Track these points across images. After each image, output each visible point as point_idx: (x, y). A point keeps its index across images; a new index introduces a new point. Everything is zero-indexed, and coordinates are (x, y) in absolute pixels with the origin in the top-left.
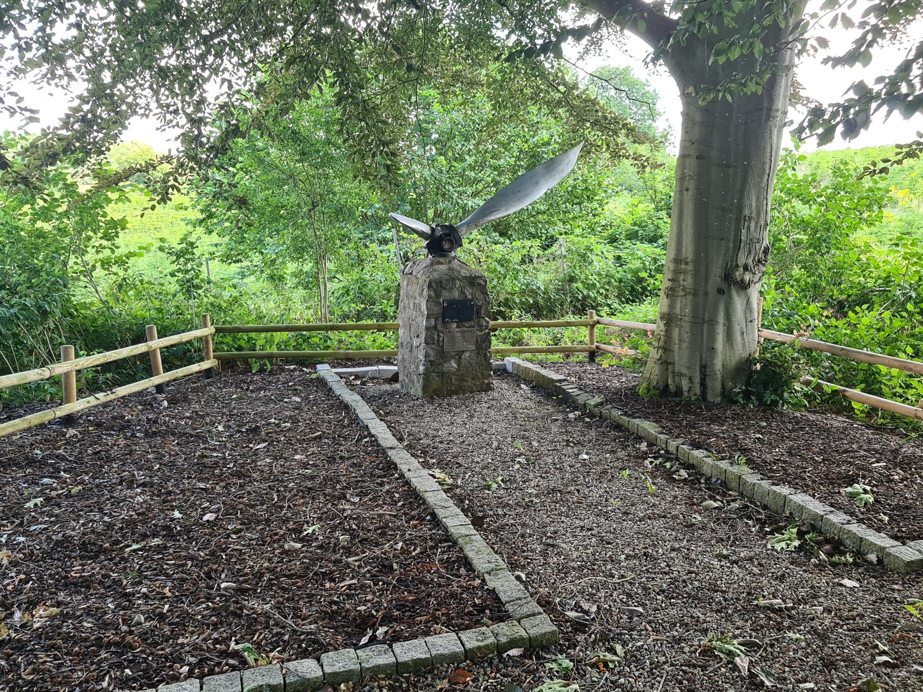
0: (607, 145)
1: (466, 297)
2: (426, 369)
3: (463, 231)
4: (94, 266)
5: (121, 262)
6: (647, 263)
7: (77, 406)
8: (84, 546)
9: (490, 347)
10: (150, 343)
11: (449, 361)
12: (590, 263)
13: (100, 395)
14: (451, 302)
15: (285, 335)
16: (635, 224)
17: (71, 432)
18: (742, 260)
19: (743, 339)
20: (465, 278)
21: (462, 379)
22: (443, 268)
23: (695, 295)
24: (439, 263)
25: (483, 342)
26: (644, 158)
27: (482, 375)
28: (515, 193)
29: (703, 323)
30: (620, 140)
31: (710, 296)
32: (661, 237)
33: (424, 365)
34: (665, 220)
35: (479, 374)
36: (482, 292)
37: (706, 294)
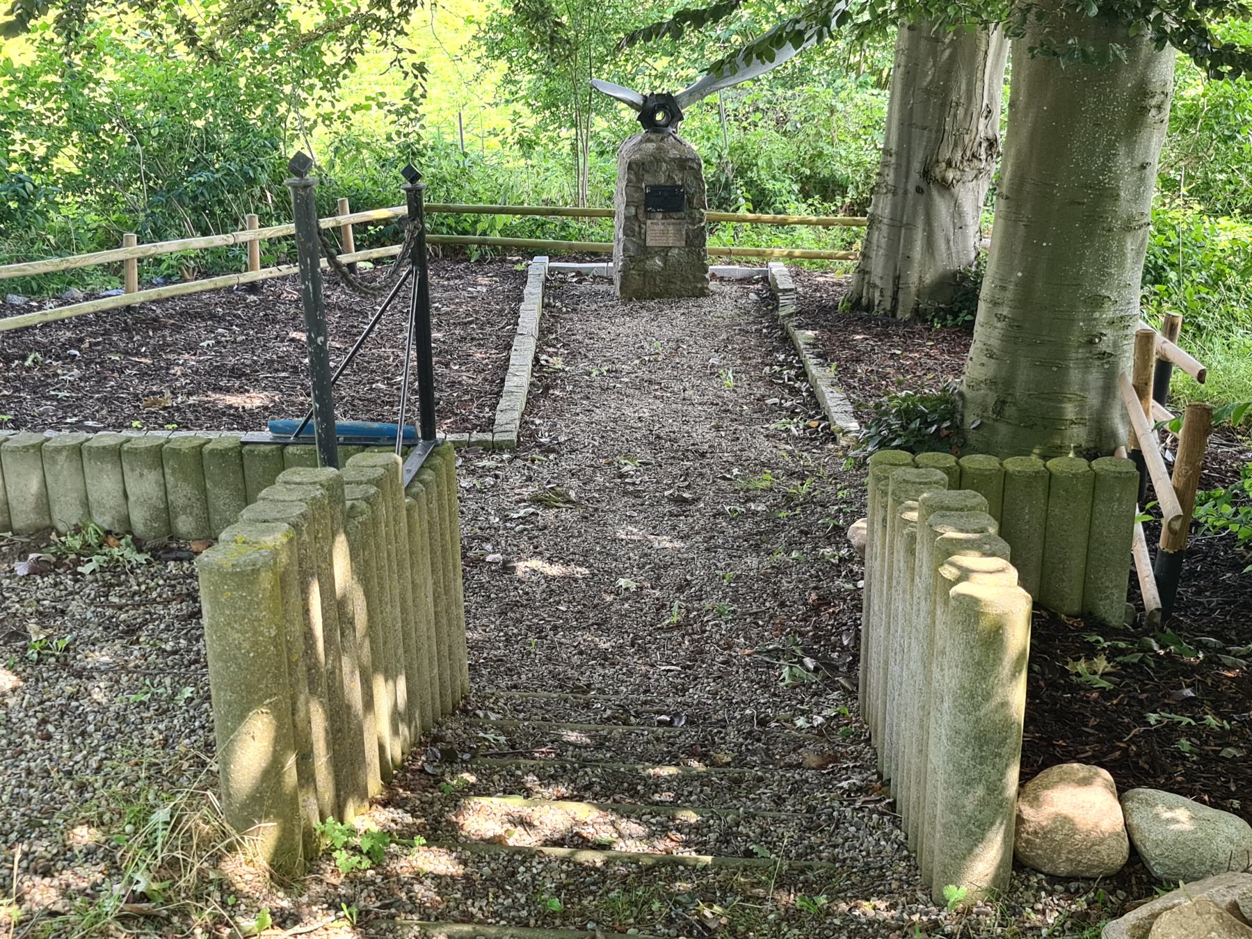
4: (315, 122)
5: (343, 117)
7: (258, 274)
8: (232, 370)
10: (339, 218)
11: (653, 258)
13: (283, 267)
14: (655, 189)
15: (516, 220)
17: (252, 298)
18: (946, 154)
19: (949, 248)
20: (674, 160)
22: (651, 146)
23: (895, 194)
29: (901, 227)
31: (910, 196)
37: (906, 192)
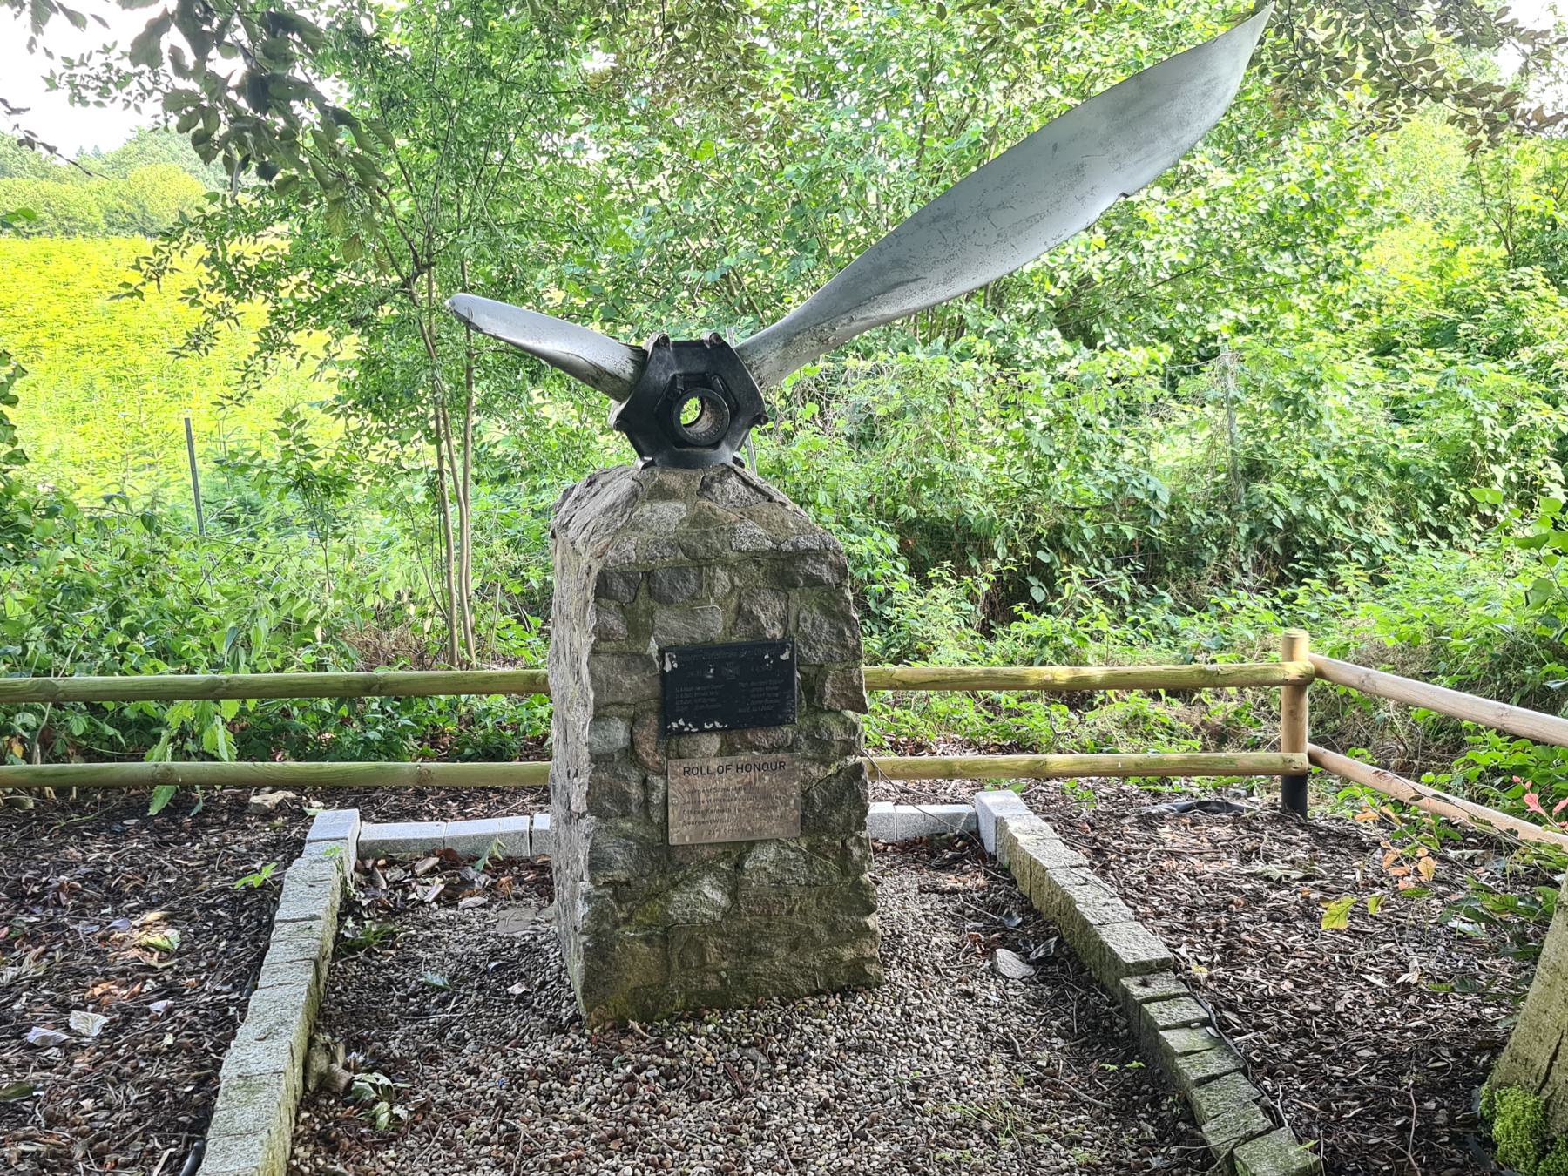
0: (1371, 55)
1: (759, 630)
2: (598, 916)
3: (763, 367)
6: (1487, 422)
9: (861, 825)
11: (691, 880)
12: (1312, 423)
14: (694, 657)
16: (1448, 302)
20: (754, 557)
21: (747, 949)
22: (670, 514)
24: (662, 493)
25: (835, 803)
26: (1498, 97)
27: (832, 929)
28: (986, 214)
30: (1412, 39)
32: (1528, 341)
33: (588, 899)
34: (1542, 292)
35: (818, 928)
36: (828, 612)
